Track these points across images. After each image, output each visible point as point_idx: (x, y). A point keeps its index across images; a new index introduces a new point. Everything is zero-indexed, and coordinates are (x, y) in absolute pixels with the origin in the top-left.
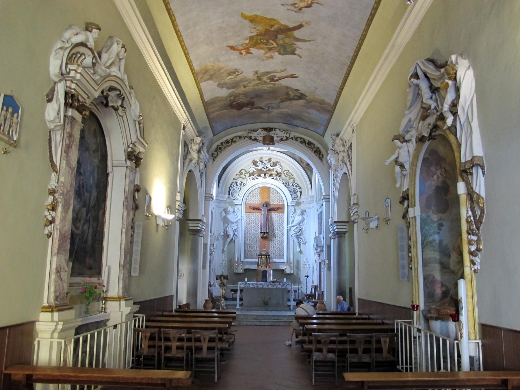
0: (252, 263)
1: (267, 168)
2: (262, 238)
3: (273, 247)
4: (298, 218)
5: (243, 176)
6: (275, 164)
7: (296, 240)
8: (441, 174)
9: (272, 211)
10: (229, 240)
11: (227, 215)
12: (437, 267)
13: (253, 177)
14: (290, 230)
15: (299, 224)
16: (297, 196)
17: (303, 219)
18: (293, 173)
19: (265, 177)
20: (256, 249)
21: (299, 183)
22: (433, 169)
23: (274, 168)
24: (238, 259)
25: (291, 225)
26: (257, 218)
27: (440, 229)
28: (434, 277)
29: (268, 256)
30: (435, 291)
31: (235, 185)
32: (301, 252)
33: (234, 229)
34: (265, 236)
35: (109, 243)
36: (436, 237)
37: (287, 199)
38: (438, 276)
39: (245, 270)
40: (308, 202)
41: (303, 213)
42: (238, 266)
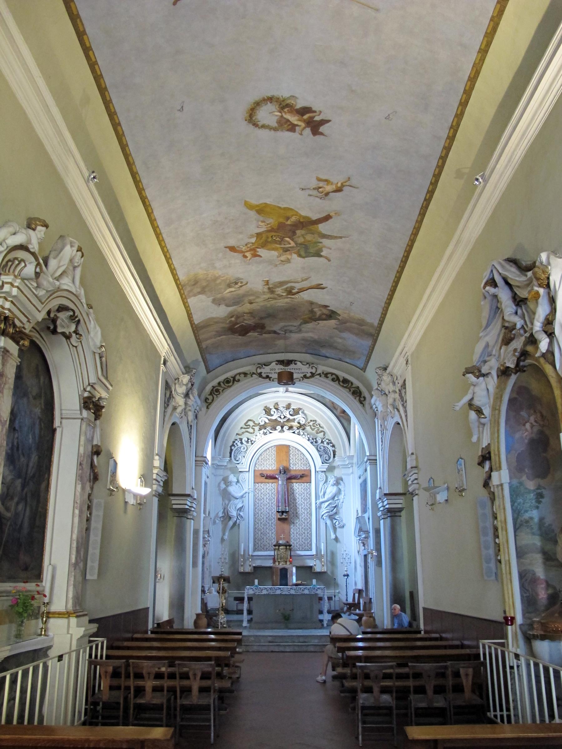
1: (285, 417)
2: (279, 519)
3: (295, 533)
4: (331, 490)
5: (251, 430)
6: (296, 412)
7: (329, 522)
8: (536, 421)
9: (293, 481)
10: (231, 523)
11: (227, 486)
12: (538, 558)
13: (265, 431)
14: (320, 507)
15: (333, 498)
16: (330, 458)
17: (339, 492)
18: (322, 425)
20: (271, 537)
22: (524, 413)
24: (244, 551)
25: (321, 500)
26: (271, 490)
27: (539, 502)
28: (534, 574)
29: (288, 546)
30: (537, 595)
31: (239, 444)
32: (336, 539)
34: (283, 517)
36: (535, 514)
37: (315, 461)
38: (540, 572)
39: (254, 567)
40: (345, 466)
41: (338, 481)
42: (244, 561)
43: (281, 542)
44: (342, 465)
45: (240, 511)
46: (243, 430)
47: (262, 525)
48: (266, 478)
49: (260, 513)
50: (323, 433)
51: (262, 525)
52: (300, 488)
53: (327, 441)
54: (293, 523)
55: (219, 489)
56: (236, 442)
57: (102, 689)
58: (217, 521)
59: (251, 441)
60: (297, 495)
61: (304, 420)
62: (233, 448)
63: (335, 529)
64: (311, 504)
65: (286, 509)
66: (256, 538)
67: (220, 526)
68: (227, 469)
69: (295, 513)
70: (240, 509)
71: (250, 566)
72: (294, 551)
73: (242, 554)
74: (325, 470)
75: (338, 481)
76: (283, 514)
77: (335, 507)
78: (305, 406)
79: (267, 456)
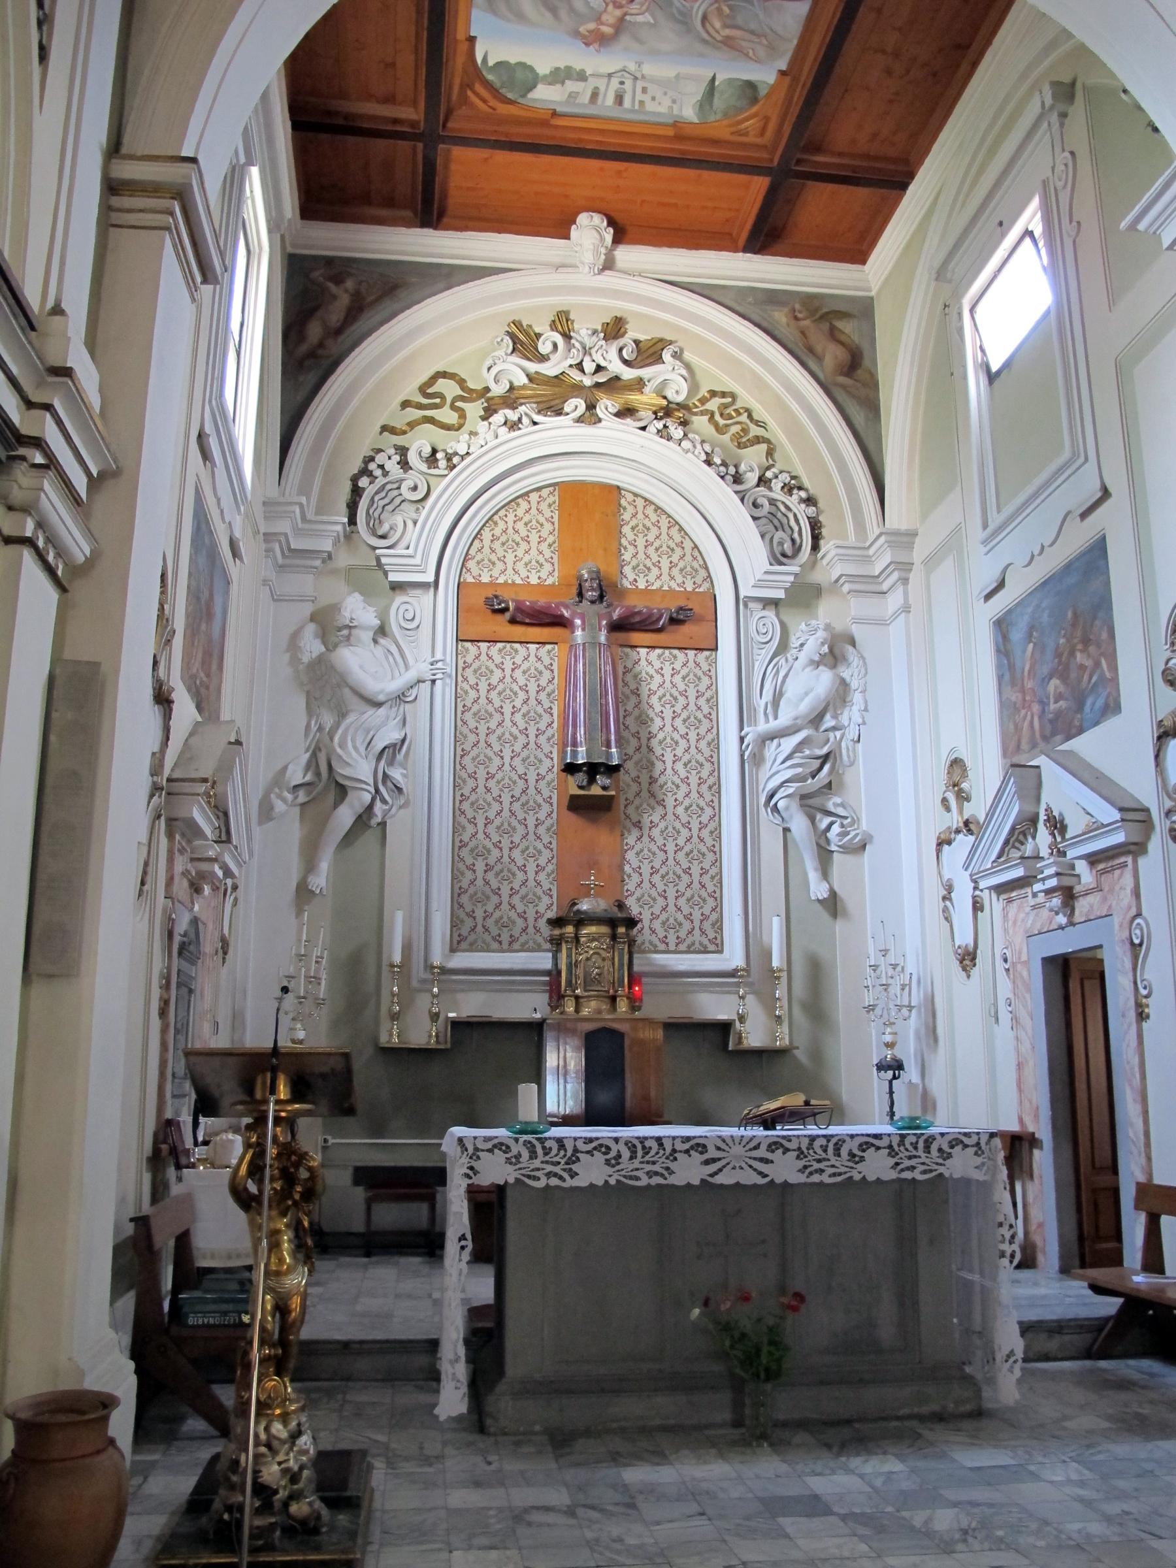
0: (506, 978)
1: (599, 369)
2: (577, 805)
3: (646, 871)
4: (806, 686)
5: (447, 415)
6: (649, 353)
7: (799, 824)
9: (637, 637)
10: (345, 816)
11: (331, 647)
13: (513, 416)
14: (758, 759)
15: (816, 720)
16: (797, 550)
17: (841, 694)
18: (760, 413)
19: (590, 416)
20: (535, 879)
21: (800, 471)
23: (645, 373)
24: (407, 948)
25: (762, 727)
26: (529, 669)
29: (620, 924)
31: (392, 466)
32: (833, 905)
33: (379, 745)
34: (595, 790)
35: (793, 948)
37: (734, 553)
39: (456, 1024)
40: (870, 586)
41: (836, 652)
42: (407, 998)
43: (584, 906)
44: (853, 578)
45: (391, 763)
46: (414, 414)
47: (491, 829)
48: (513, 621)
49: (481, 774)
50: (763, 447)
51: (491, 829)
52: (667, 671)
53: (785, 477)
54: (638, 825)
55: (295, 660)
56: (380, 458)
57: (1141, 227)
58: (280, 806)
59: (449, 458)
60: (654, 700)
61: (684, 387)
62: (363, 482)
63: (824, 855)
64: (715, 745)
65: (609, 755)
66: (462, 892)
67: (292, 829)
68: (334, 572)
69: (644, 780)
70: (391, 752)
71: (435, 1017)
72: (644, 952)
73: (397, 958)
74: (781, 594)
75: (836, 652)
76: (592, 780)
77: (825, 758)
78: (685, 331)
79: (520, 526)
